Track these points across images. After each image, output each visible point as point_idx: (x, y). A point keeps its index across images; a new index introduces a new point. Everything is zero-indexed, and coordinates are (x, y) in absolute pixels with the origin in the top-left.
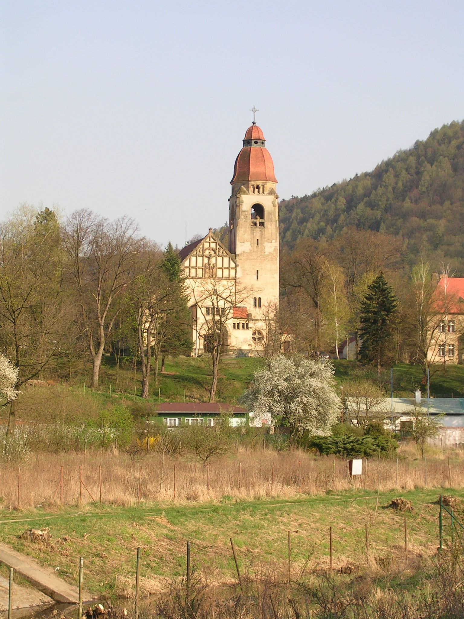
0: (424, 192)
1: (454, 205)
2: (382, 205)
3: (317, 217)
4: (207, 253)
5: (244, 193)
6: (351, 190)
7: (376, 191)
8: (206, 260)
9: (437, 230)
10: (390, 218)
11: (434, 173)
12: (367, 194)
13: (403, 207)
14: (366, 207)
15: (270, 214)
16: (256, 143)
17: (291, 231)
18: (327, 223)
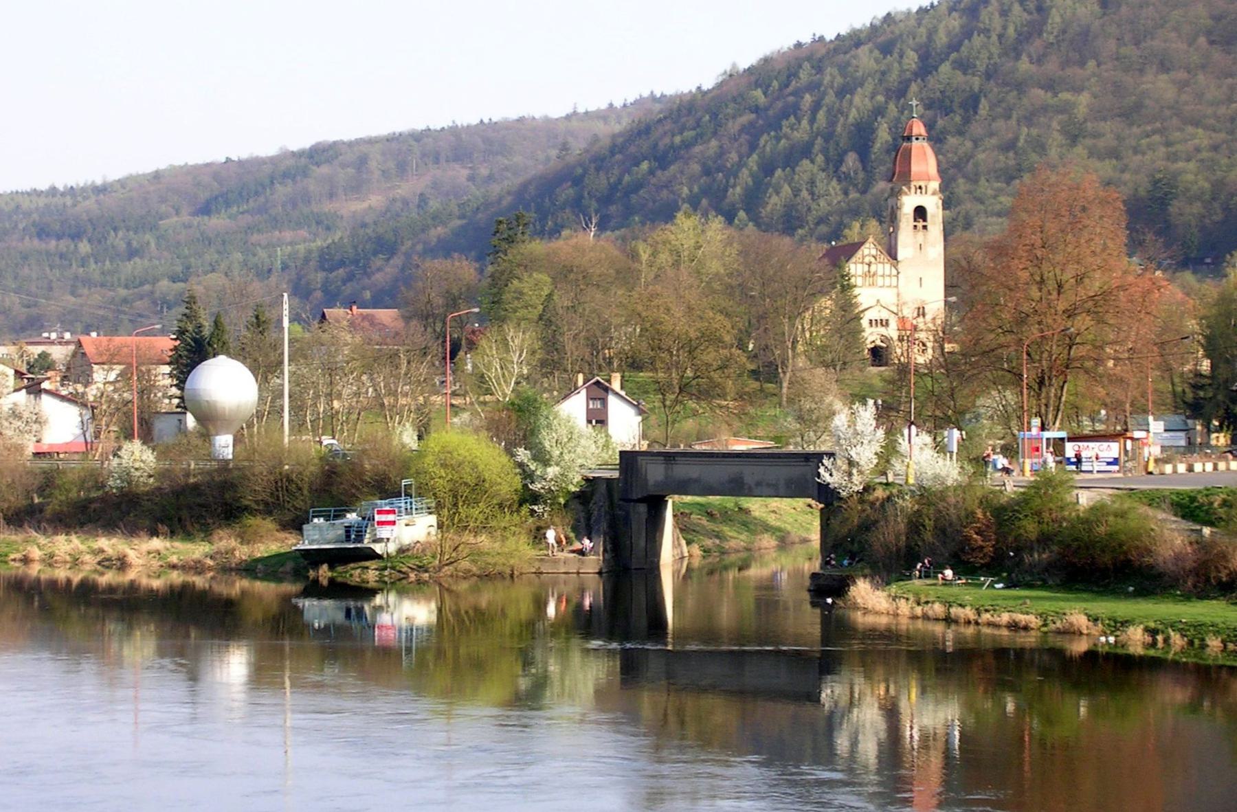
0: (1052, 44)
1: (1103, 67)
2: (981, 66)
3: (869, 87)
4: (867, 260)
5: (906, 194)
6: (924, 36)
7: (970, 41)
8: (866, 268)
9: (1075, 111)
10: (995, 90)
11: (1068, 11)
12: (954, 47)
13: (1018, 70)
14: (954, 69)
15: (933, 216)
16: (917, 139)
17: (825, 109)
18: (888, 98)
